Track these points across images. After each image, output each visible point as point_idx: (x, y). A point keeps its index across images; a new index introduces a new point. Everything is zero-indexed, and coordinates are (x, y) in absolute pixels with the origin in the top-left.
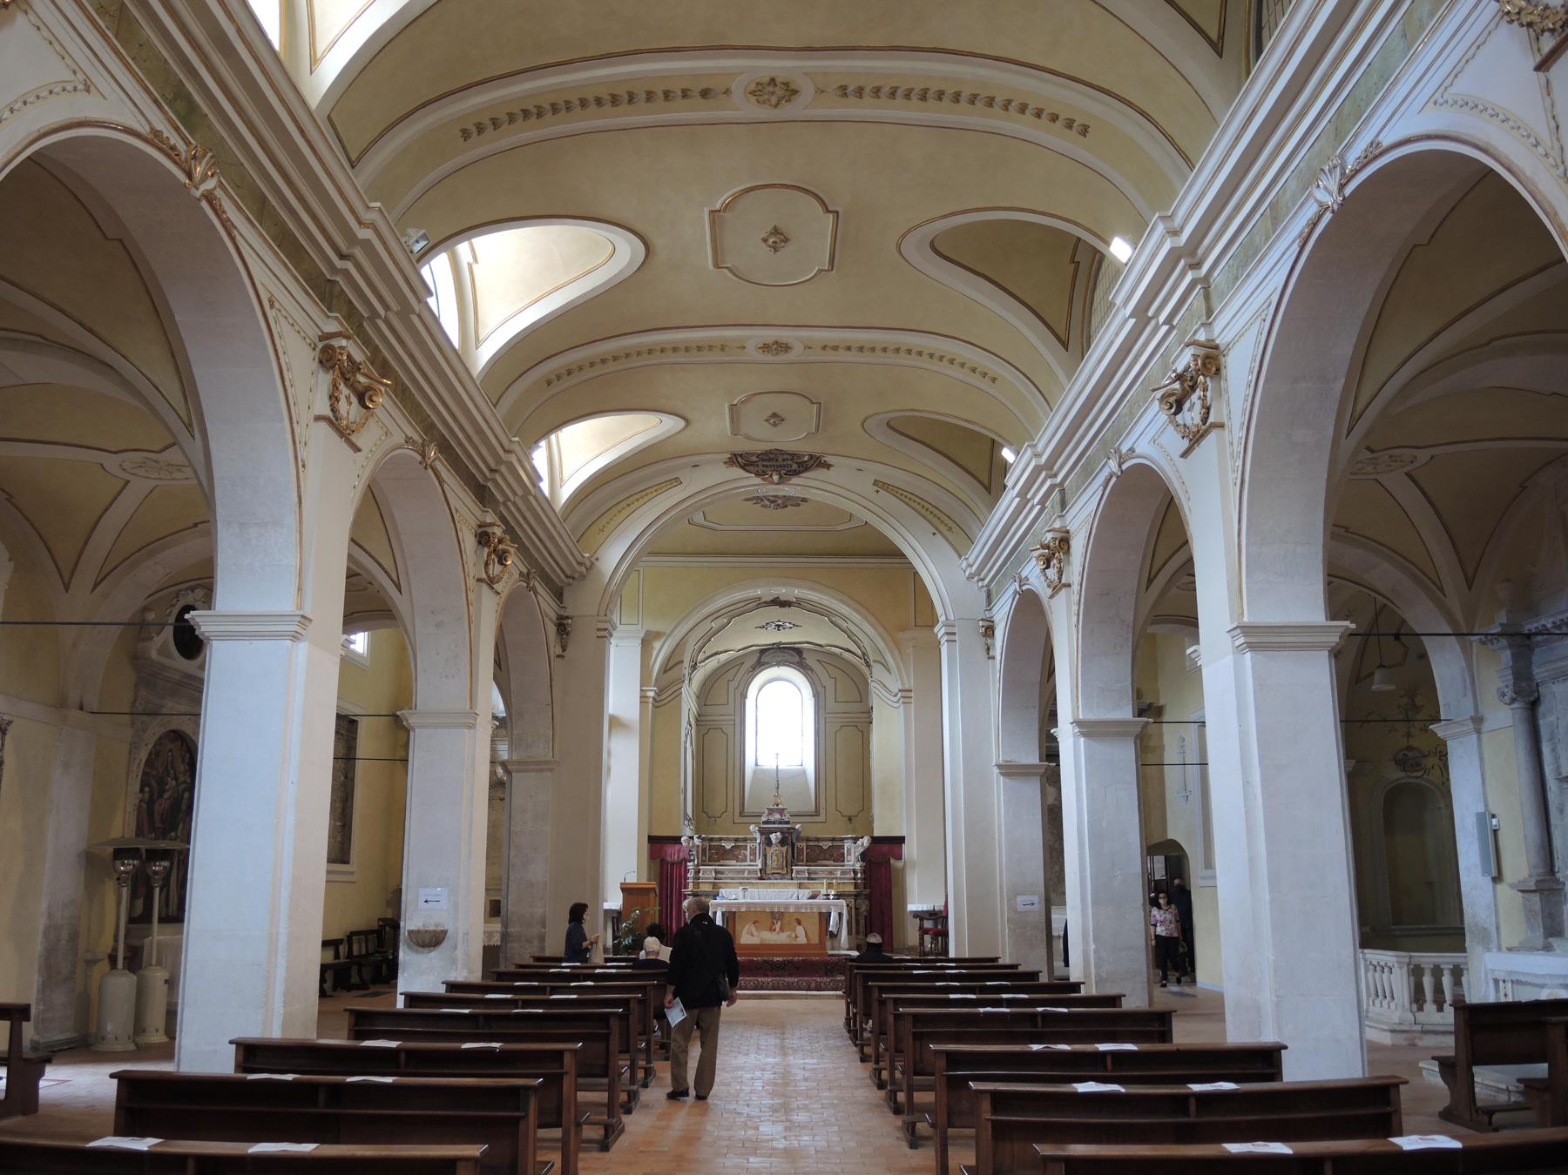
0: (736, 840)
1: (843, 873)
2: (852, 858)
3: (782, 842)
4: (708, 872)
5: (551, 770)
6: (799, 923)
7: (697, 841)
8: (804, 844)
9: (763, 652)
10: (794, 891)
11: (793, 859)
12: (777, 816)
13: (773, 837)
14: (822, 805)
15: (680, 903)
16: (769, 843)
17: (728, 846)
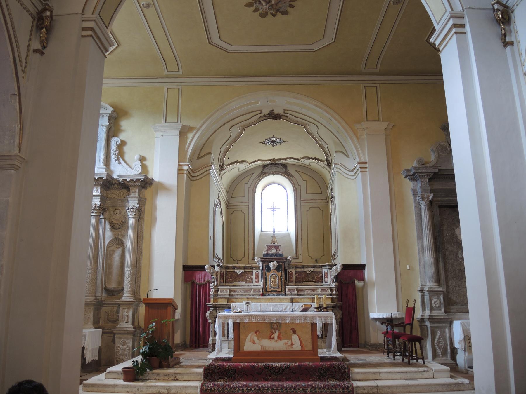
0: (245, 268)
1: (323, 290)
2: (329, 280)
3: (278, 269)
4: (224, 291)
5: (16, 168)
6: (294, 332)
7: (217, 269)
8: (293, 270)
9: (265, 166)
10: (289, 305)
11: (286, 281)
12: (274, 251)
13: (271, 265)
14: (300, 252)
15: (205, 312)
16: (268, 269)
17: (239, 272)
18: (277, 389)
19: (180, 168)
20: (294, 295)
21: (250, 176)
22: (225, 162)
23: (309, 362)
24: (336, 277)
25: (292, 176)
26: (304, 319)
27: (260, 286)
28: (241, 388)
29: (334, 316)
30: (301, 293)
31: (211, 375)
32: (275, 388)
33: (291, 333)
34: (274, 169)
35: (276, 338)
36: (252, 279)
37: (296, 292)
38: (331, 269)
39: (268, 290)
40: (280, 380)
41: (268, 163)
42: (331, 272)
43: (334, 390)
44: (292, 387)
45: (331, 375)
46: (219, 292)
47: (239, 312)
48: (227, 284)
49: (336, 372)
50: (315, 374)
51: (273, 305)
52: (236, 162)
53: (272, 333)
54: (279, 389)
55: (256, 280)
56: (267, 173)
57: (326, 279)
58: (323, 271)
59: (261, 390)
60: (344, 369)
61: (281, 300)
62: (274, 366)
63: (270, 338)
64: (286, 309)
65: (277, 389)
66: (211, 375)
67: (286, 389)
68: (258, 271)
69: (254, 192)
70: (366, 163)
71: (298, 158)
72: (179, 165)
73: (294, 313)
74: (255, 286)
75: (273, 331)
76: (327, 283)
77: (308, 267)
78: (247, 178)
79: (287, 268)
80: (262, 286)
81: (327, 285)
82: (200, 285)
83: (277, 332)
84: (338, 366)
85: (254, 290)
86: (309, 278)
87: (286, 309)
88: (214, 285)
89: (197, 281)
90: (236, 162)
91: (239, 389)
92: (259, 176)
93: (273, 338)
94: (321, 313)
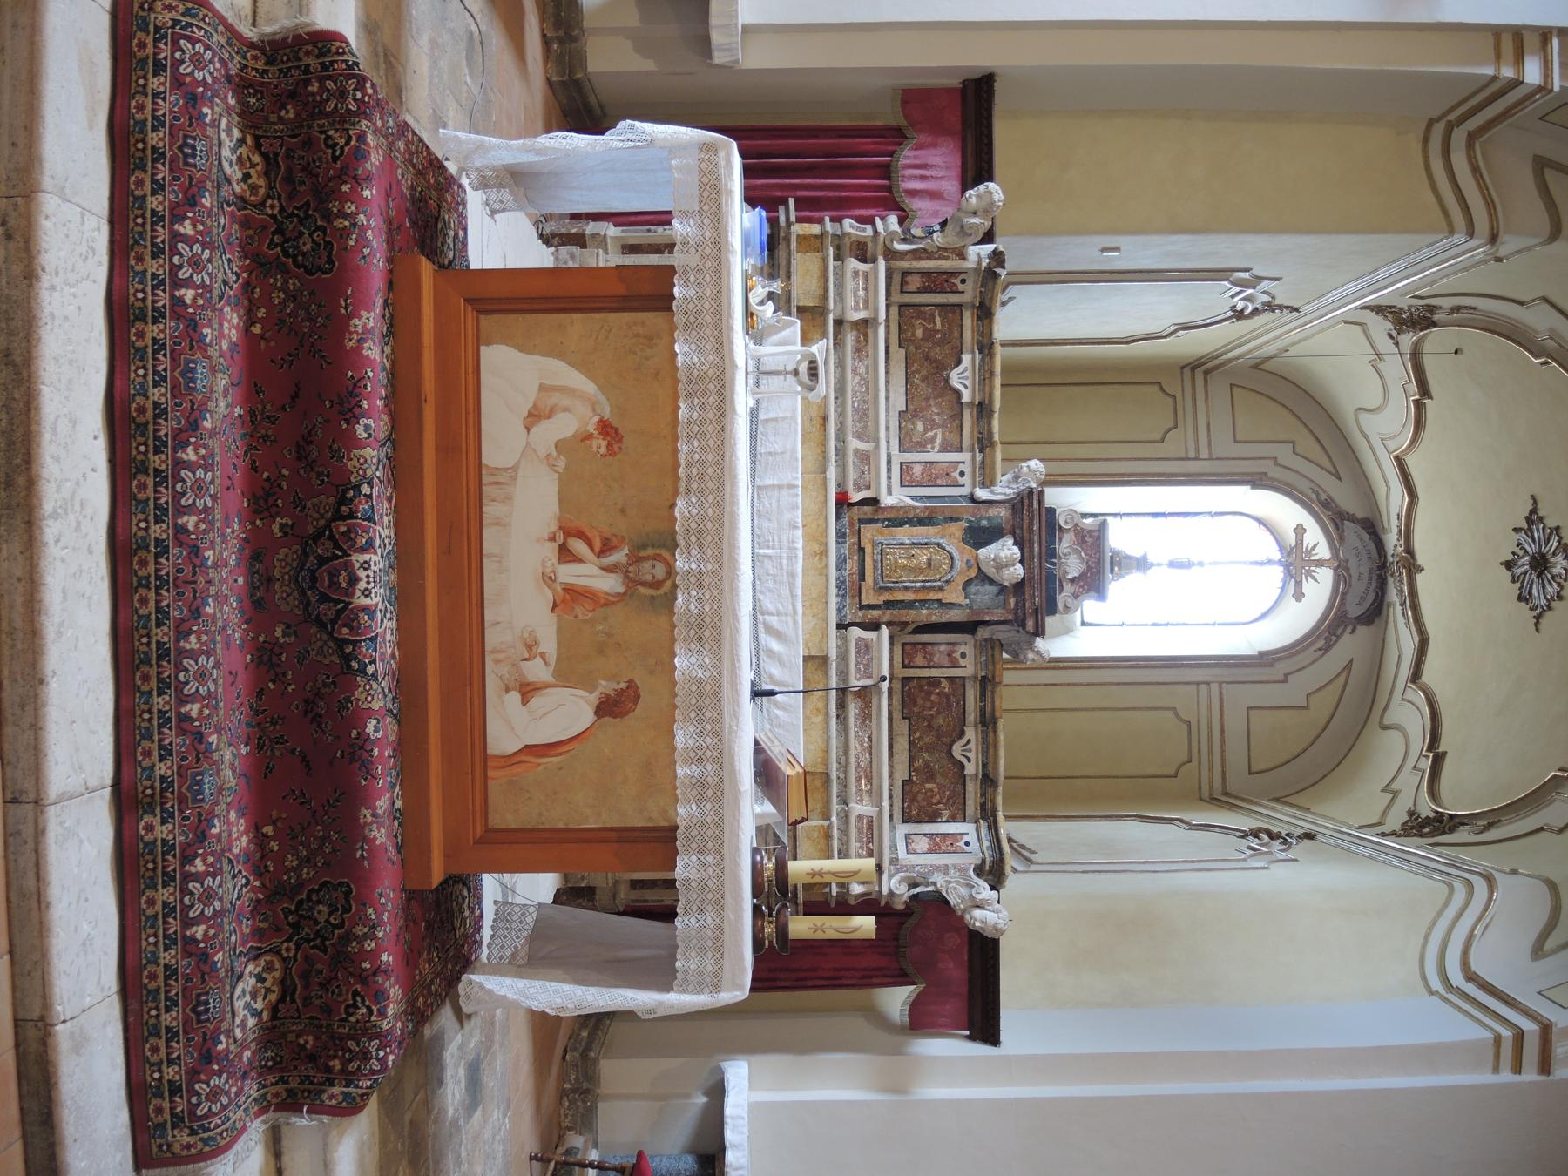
0: (983, 409)
4: (863, 291)
6: (608, 708)
9: (1372, 528)
12: (1073, 566)
13: (1006, 549)
16: (980, 536)
17: (962, 378)
18: (162, 583)
19: (1531, 41)
20: (843, 674)
21: (1326, 462)
22: (1437, 340)
23: (394, 814)
24: (939, 902)
25: (1327, 649)
26: (701, 784)
27: (890, 493)
28: (163, 299)
29: (728, 997)
30: (853, 708)
31: (293, 95)
32: (167, 566)
33: (606, 687)
34: (1361, 569)
35: (569, 574)
36: (921, 446)
37: (855, 683)
38: (979, 871)
39: (868, 532)
40: (258, 605)
41: (1392, 540)
42: (961, 870)
43: (167, 1019)
44: (183, 700)
45: (305, 976)
46: (853, 264)
47: (749, 314)
48: (894, 311)
49: (328, 1011)
50: (308, 860)
51: (792, 558)
52: (1424, 391)
53: (606, 548)
54: (167, 598)
55: (917, 469)
56: (1341, 538)
57: (923, 844)
58: (966, 829)
59: (155, 461)
60: (349, 1078)
61: (816, 602)
62: (357, 558)
63: (568, 533)
64: (771, 630)
65: (162, 583)
66: (293, 95)
67: (163, 653)
68: (966, 480)
69: (1258, 481)
70: (1545, 1067)
71: (1426, 677)
72: (1545, 34)
73: (747, 705)
74: (889, 462)
75: (620, 556)
76: (901, 845)
77: (989, 747)
78: (1316, 452)
79: (983, 633)
80: (887, 500)
81: (894, 847)
82: (886, 171)
83: (610, 584)
84: (367, 1031)
85: (865, 458)
86: (930, 748)
87: (771, 630)
88: (892, 236)
89: (907, 155)
90: (1424, 391)
91: (158, 283)
92: (1327, 504)
93: (565, 554)
94: (748, 902)
